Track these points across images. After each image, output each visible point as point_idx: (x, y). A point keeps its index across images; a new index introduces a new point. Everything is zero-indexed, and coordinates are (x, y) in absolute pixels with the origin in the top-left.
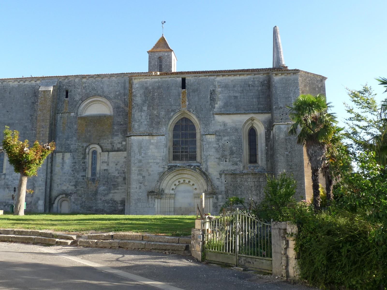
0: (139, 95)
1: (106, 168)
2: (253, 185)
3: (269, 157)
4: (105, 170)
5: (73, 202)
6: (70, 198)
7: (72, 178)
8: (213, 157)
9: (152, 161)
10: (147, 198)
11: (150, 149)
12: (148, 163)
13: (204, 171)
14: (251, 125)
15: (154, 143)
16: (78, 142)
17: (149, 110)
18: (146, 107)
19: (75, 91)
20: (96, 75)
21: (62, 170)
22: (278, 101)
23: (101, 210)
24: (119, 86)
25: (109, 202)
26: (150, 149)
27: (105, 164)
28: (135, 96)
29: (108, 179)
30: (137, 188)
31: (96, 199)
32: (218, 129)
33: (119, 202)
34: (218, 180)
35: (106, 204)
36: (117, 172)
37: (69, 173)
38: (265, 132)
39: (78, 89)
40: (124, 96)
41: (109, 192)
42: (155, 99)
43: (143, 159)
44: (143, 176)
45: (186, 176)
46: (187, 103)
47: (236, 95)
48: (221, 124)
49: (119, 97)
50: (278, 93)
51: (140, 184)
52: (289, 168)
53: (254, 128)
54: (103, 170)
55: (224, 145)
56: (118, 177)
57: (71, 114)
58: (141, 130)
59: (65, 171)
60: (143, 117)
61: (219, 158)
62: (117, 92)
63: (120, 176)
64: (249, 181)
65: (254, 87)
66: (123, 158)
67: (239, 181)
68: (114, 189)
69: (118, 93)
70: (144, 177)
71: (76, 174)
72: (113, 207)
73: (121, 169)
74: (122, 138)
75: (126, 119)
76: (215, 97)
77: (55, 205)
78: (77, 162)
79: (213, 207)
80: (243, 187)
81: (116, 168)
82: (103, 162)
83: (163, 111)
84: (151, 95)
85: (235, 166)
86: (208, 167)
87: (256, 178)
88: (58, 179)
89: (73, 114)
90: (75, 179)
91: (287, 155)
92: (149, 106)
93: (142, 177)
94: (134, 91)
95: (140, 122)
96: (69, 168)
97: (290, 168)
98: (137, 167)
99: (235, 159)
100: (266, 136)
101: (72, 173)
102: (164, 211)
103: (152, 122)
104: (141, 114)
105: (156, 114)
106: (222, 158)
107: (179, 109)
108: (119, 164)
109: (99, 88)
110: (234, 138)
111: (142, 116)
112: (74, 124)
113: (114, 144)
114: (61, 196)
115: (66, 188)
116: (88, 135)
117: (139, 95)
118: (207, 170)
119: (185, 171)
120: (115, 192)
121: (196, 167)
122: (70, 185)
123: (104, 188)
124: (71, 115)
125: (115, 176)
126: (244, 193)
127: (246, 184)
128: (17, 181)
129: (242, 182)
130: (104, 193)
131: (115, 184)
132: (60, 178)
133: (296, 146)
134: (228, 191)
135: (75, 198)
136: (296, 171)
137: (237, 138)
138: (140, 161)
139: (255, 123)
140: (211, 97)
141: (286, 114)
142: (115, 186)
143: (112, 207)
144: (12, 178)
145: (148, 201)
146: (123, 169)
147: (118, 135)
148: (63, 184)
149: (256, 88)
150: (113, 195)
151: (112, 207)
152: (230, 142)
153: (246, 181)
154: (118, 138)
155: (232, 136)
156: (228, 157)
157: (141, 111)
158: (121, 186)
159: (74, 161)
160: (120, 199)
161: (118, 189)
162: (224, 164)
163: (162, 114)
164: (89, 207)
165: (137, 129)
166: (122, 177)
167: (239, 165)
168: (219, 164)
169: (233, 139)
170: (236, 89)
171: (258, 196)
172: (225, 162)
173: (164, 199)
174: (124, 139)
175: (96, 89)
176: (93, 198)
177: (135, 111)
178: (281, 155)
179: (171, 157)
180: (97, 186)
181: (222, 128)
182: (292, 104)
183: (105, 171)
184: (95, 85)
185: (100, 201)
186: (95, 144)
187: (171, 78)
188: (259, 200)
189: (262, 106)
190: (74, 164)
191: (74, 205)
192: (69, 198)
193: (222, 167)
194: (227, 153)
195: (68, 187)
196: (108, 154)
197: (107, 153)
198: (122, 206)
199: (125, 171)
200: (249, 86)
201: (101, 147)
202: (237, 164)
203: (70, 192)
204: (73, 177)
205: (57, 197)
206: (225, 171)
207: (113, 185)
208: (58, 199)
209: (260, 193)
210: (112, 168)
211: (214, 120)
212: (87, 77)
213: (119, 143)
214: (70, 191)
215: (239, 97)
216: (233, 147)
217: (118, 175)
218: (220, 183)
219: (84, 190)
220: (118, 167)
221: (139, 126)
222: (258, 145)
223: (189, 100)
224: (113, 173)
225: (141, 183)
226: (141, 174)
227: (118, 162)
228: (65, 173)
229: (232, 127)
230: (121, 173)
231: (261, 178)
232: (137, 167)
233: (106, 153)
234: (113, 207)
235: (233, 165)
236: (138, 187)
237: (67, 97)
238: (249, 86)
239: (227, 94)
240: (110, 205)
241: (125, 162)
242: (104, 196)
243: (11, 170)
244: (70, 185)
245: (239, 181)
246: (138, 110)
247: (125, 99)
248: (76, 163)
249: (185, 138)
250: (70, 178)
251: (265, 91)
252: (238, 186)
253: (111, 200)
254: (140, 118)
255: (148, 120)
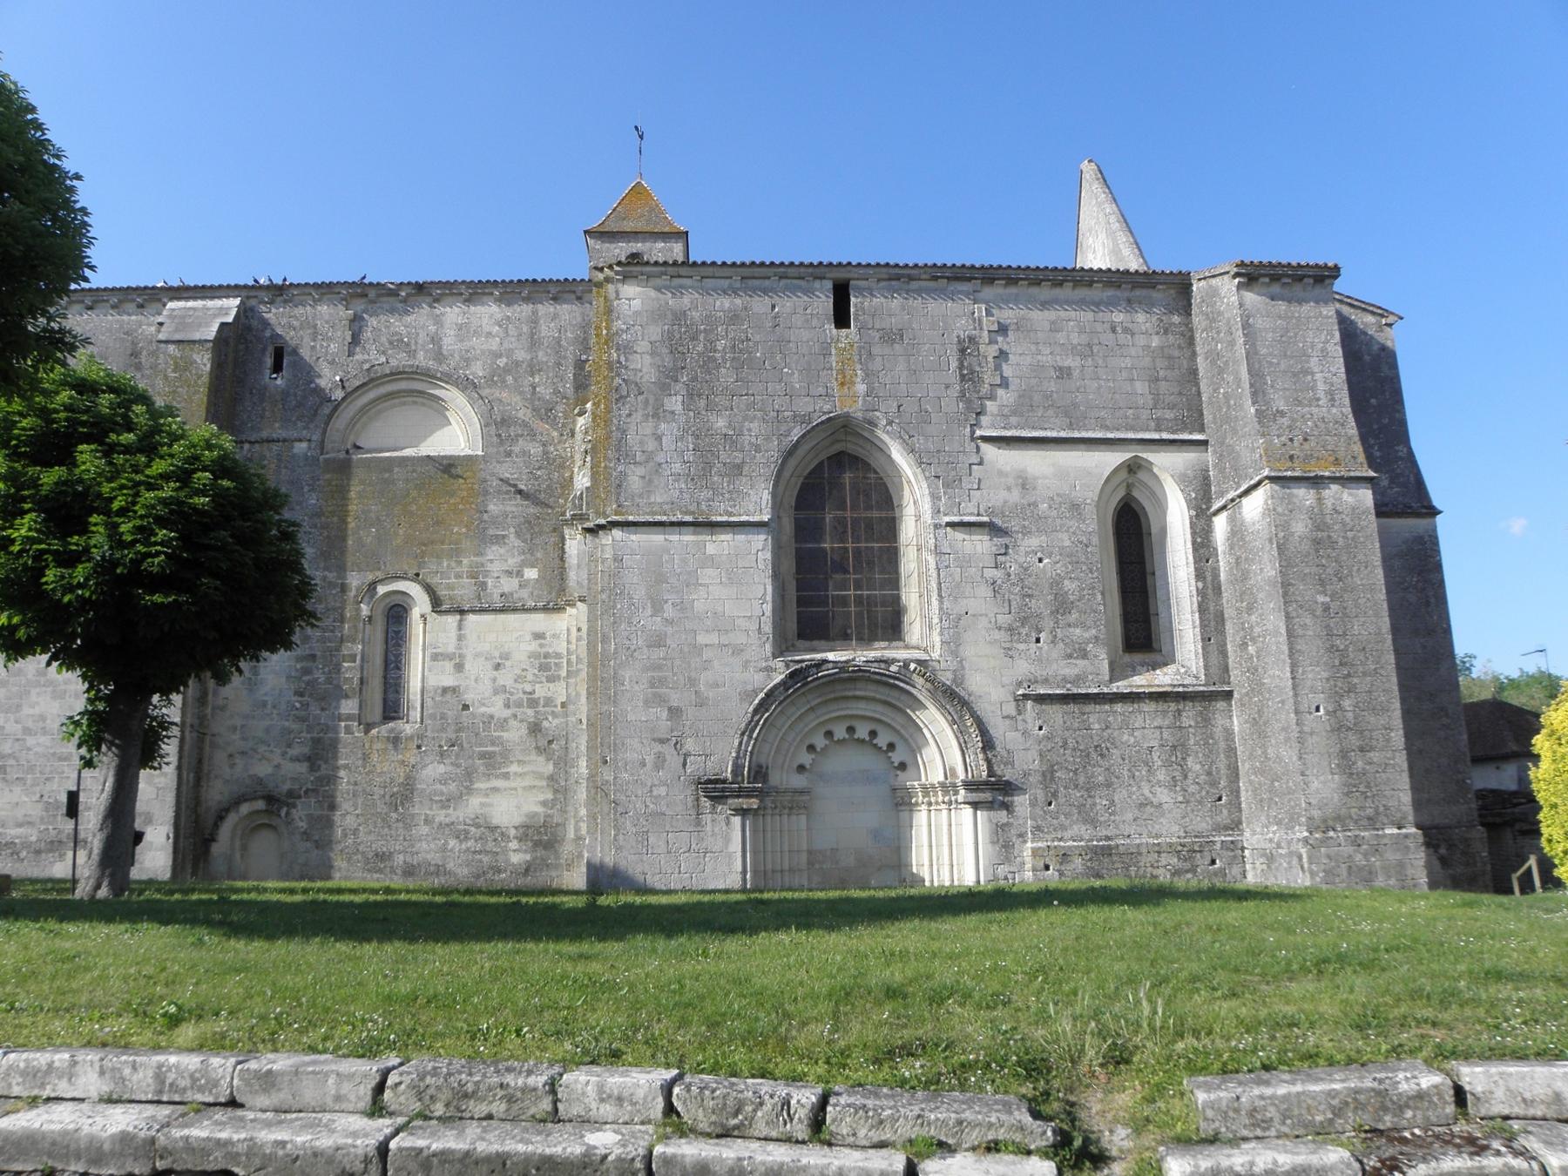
0: (642, 346)
1: (449, 681)
2: (1155, 743)
3: (1213, 623)
4: (445, 690)
5: (305, 833)
6: (287, 814)
7: (295, 726)
8: (983, 622)
9: (713, 638)
10: (693, 812)
11: (701, 585)
12: (698, 649)
13: (948, 683)
14: (1121, 493)
15: (720, 555)
16: (326, 569)
17: (692, 414)
18: (680, 398)
19: (313, 348)
20: (409, 283)
21: (251, 690)
22: (1266, 384)
23: (432, 868)
24: (510, 333)
25: (467, 832)
26: (701, 585)
27: (448, 666)
28: (625, 348)
29: (458, 730)
30: (643, 764)
31: (407, 822)
32: (999, 504)
33: (513, 832)
34: (1008, 722)
35: (452, 843)
36: (499, 701)
37: (283, 707)
38: (1191, 518)
39: (330, 339)
40: (532, 375)
41: (467, 788)
42: (718, 367)
43: (670, 630)
44: (670, 709)
45: (861, 708)
46: (861, 388)
47: (1066, 364)
48: (1011, 481)
49: (510, 379)
50: (1264, 351)
51: (658, 747)
52: (1337, 662)
53: (1133, 505)
54: (439, 691)
55: (1026, 569)
56: (505, 720)
57: (297, 445)
58: (659, 500)
59: (266, 694)
60: (664, 438)
61: (1010, 629)
62: (501, 356)
63: (515, 716)
64: (1137, 725)
65: (1133, 334)
66: (528, 637)
67: (1097, 726)
68: (488, 776)
69: (505, 360)
70: (675, 712)
71: (315, 710)
72: (487, 852)
73: (520, 686)
74: (524, 553)
75: (539, 468)
76: (978, 369)
77: (217, 849)
78: (319, 653)
79: (993, 843)
80: (1115, 751)
81: (494, 680)
82: (435, 657)
83: (755, 416)
84: (700, 348)
85: (1078, 662)
86: (963, 668)
87: (1165, 712)
88: (234, 729)
89: (304, 445)
90: (310, 729)
91: (1326, 608)
92: (691, 395)
93: (665, 714)
94: (624, 327)
95: (651, 464)
96: (283, 680)
97: (1341, 664)
98: (646, 669)
99: (1078, 631)
100: (1194, 534)
101: (298, 705)
102: (769, 867)
103: (708, 466)
104: (656, 427)
105: (724, 431)
106: (1023, 625)
107: (825, 413)
108: (508, 663)
109: (422, 335)
110: (1067, 543)
111: (659, 438)
112: (306, 489)
113: (486, 576)
114: (245, 808)
115: (270, 770)
116: (370, 538)
117: (642, 346)
118: (959, 679)
119: (859, 685)
120: (495, 790)
121: (912, 666)
122: (288, 756)
123: (441, 769)
124: (295, 451)
125: (492, 717)
126: (1118, 778)
127: (1125, 737)
128: (42, 739)
129: (1109, 731)
130: (442, 794)
131: (494, 752)
132: (243, 726)
133: (1355, 568)
134: (1053, 772)
135: (310, 816)
136: (1365, 674)
137: (1081, 542)
138: (658, 641)
139: (1141, 481)
140: (961, 367)
141: (1306, 440)
142: (494, 761)
143: (480, 852)
144: (19, 726)
145: (698, 823)
146: (528, 688)
147: (504, 537)
148: (255, 750)
149: (1141, 340)
150: (484, 800)
151: (480, 852)
152: (1050, 557)
153: (1125, 725)
154: (502, 551)
155: (1060, 535)
156: (1048, 623)
157: (658, 414)
158: (519, 761)
159: (307, 652)
160: (518, 819)
161: (506, 776)
162: (1032, 651)
163: (750, 430)
164: (377, 855)
165: (641, 496)
166: (522, 721)
167: (1095, 656)
168: (1008, 653)
169: (1063, 548)
170: (1061, 337)
171: (1178, 788)
172: (1033, 646)
173: (770, 811)
174: (528, 556)
175: (408, 344)
176: (394, 815)
177: (629, 415)
178: (1301, 607)
179: (792, 626)
180: (413, 761)
181: (1015, 497)
182: (1318, 399)
183: (448, 696)
184: (406, 327)
185: (425, 830)
186: (397, 578)
187: (787, 278)
188: (1183, 806)
189: (1169, 415)
190: (304, 664)
191: (308, 844)
192: (283, 814)
193: (1023, 668)
194: (1041, 605)
195: (278, 766)
196: (461, 620)
197: (458, 617)
198: (526, 851)
199: (536, 696)
200: (1114, 330)
201: (430, 590)
202: (1084, 655)
203: (286, 787)
204: (303, 720)
205: (227, 810)
206: (1036, 682)
207: (483, 756)
208: (231, 819)
209: (1186, 777)
210: (476, 680)
211: (980, 464)
212: (372, 293)
213: (509, 573)
214: (288, 782)
215: (1076, 373)
216: (1066, 582)
217: (507, 713)
218: (1018, 735)
219: (352, 781)
220: (506, 678)
221: (648, 481)
222: (1154, 574)
223: (867, 375)
224: (484, 705)
225: (662, 741)
226: (660, 700)
227: (506, 656)
228: (264, 704)
229: (1058, 495)
230: (519, 705)
231: (1184, 714)
232: (646, 669)
233: (452, 620)
234: (487, 852)
235: (1070, 656)
236: (649, 759)
237: (277, 367)
238: (1114, 330)
239: (1029, 359)
240: (470, 843)
241: (533, 655)
242: (443, 807)
243: (15, 689)
244: (288, 756)
245: (1097, 726)
246: (640, 413)
247: (534, 388)
248: (313, 657)
249: (857, 539)
250: (287, 724)
251: (1176, 353)
252: (1096, 747)
253: (478, 826)
254: (651, 445)
255: (689, 456)
